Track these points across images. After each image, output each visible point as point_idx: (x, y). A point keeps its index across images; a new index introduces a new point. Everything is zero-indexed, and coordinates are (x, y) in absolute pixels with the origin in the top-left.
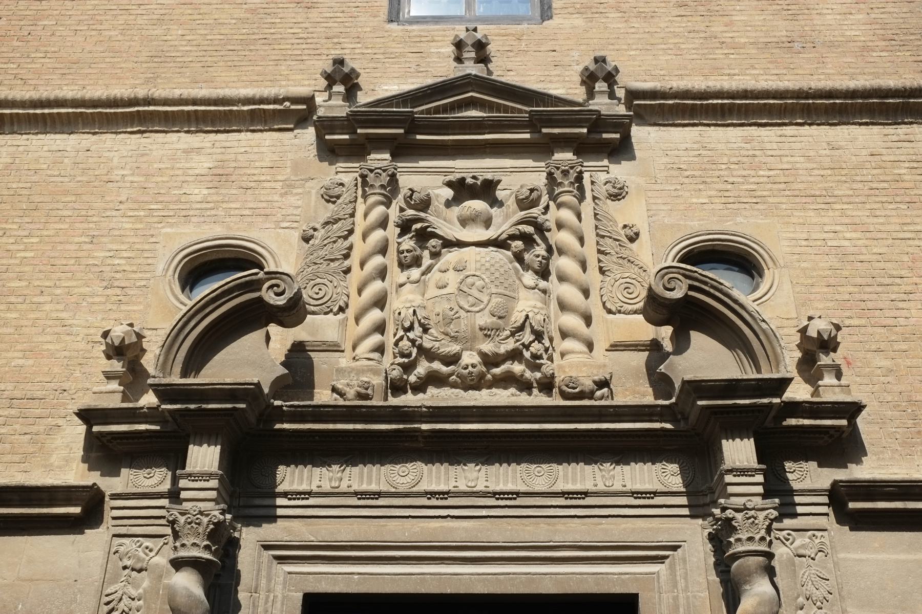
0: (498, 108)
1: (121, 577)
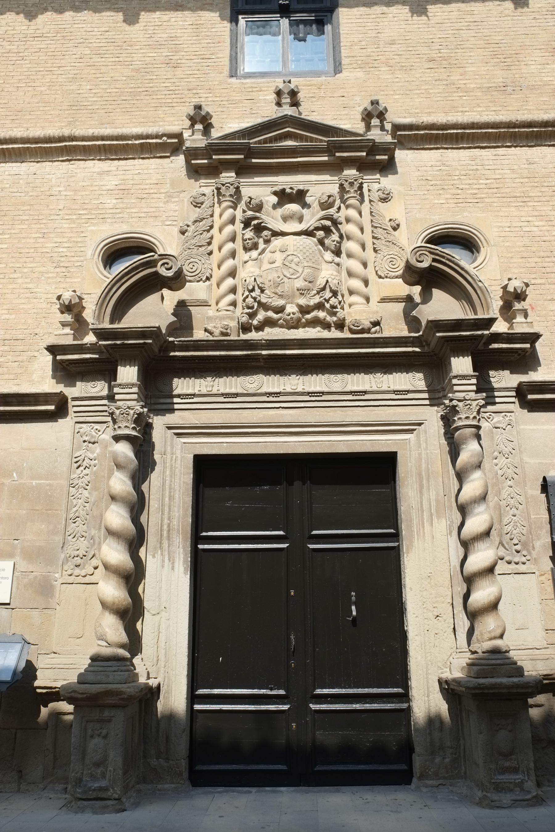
0: (307, 139)
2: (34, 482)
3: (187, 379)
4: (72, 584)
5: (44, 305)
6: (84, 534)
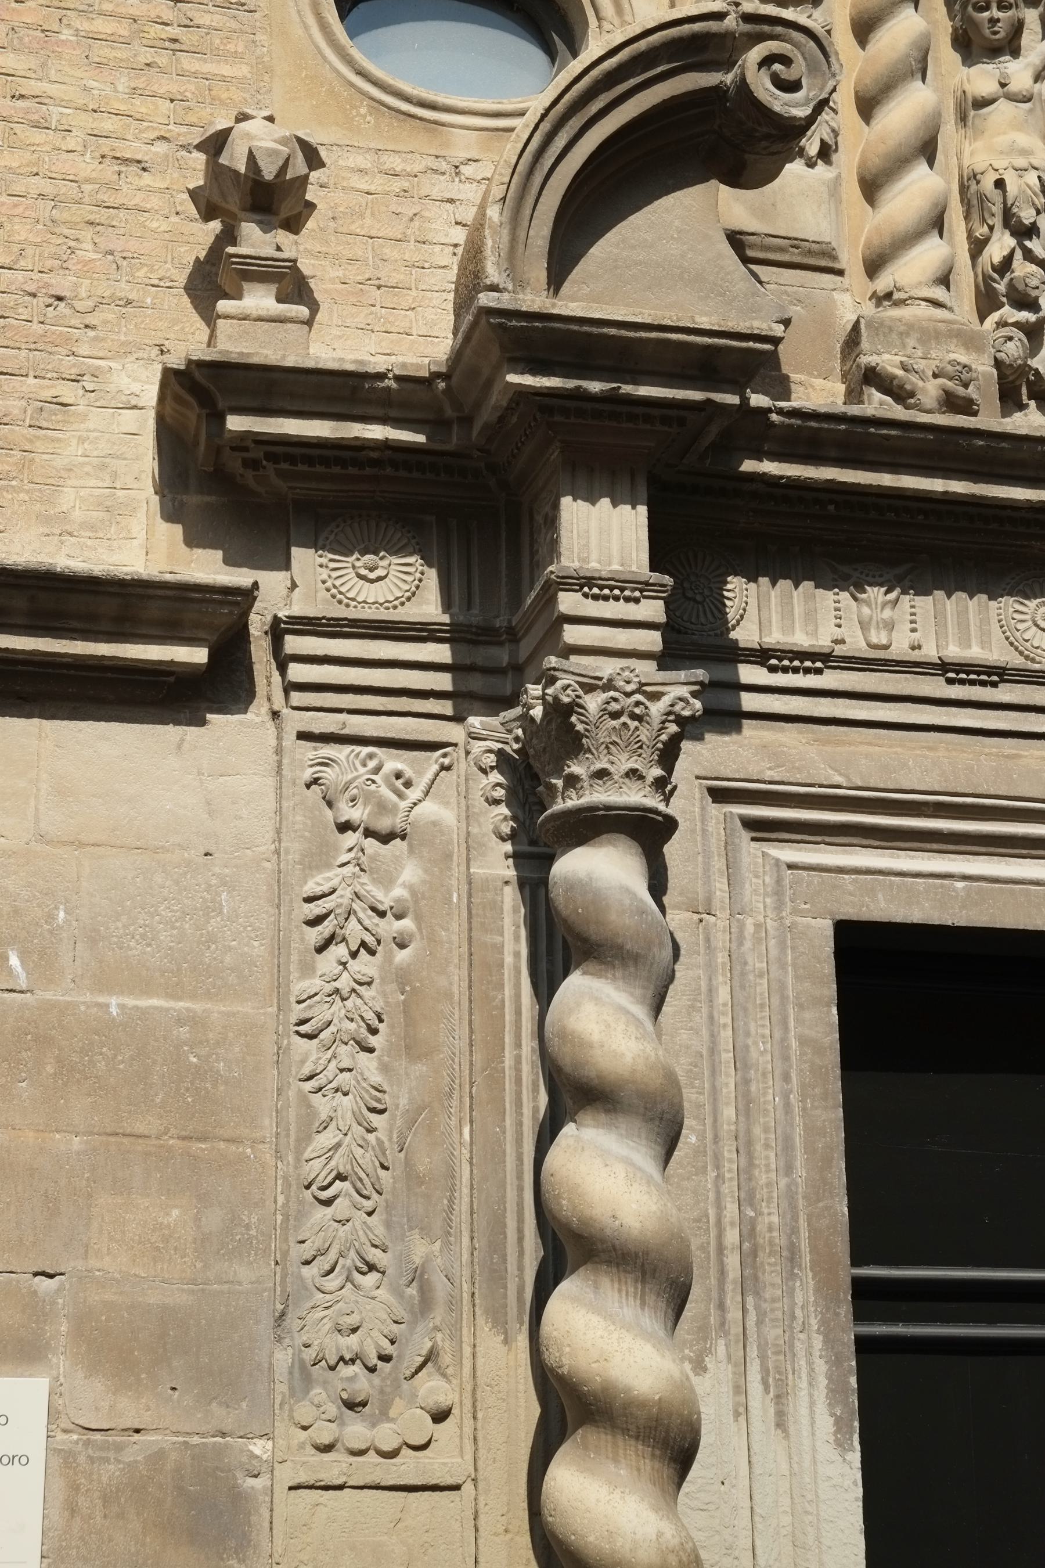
1: (337, 850)
2: (114, 1002)
3: (785, 584)
4: (340, 1487)
5: (86, 166)
6: (375, 1255)
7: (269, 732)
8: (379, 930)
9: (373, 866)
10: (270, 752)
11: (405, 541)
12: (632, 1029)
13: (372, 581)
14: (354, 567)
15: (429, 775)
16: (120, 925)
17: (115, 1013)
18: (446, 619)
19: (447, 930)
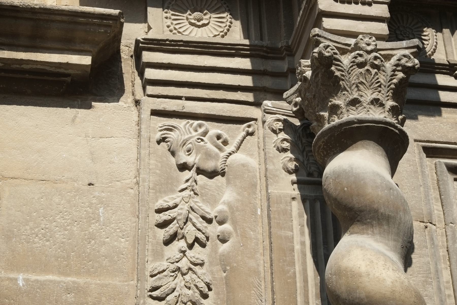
1: (178, 182)
2: (21, 278)
7: (133, 113)
8: (207, 231)
9: (203, 192)
10: (134, 124)
11: (220, 5)
12: (389, 264)
13: (199, 27)
14: (187, 19)
15: (240, 137)
16: (28, 228)
17: (21, 285)
18: (247, 42)
19: (254, 231)
